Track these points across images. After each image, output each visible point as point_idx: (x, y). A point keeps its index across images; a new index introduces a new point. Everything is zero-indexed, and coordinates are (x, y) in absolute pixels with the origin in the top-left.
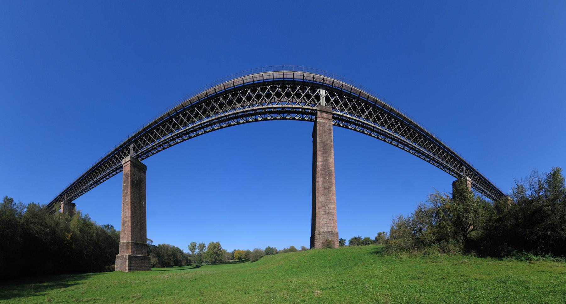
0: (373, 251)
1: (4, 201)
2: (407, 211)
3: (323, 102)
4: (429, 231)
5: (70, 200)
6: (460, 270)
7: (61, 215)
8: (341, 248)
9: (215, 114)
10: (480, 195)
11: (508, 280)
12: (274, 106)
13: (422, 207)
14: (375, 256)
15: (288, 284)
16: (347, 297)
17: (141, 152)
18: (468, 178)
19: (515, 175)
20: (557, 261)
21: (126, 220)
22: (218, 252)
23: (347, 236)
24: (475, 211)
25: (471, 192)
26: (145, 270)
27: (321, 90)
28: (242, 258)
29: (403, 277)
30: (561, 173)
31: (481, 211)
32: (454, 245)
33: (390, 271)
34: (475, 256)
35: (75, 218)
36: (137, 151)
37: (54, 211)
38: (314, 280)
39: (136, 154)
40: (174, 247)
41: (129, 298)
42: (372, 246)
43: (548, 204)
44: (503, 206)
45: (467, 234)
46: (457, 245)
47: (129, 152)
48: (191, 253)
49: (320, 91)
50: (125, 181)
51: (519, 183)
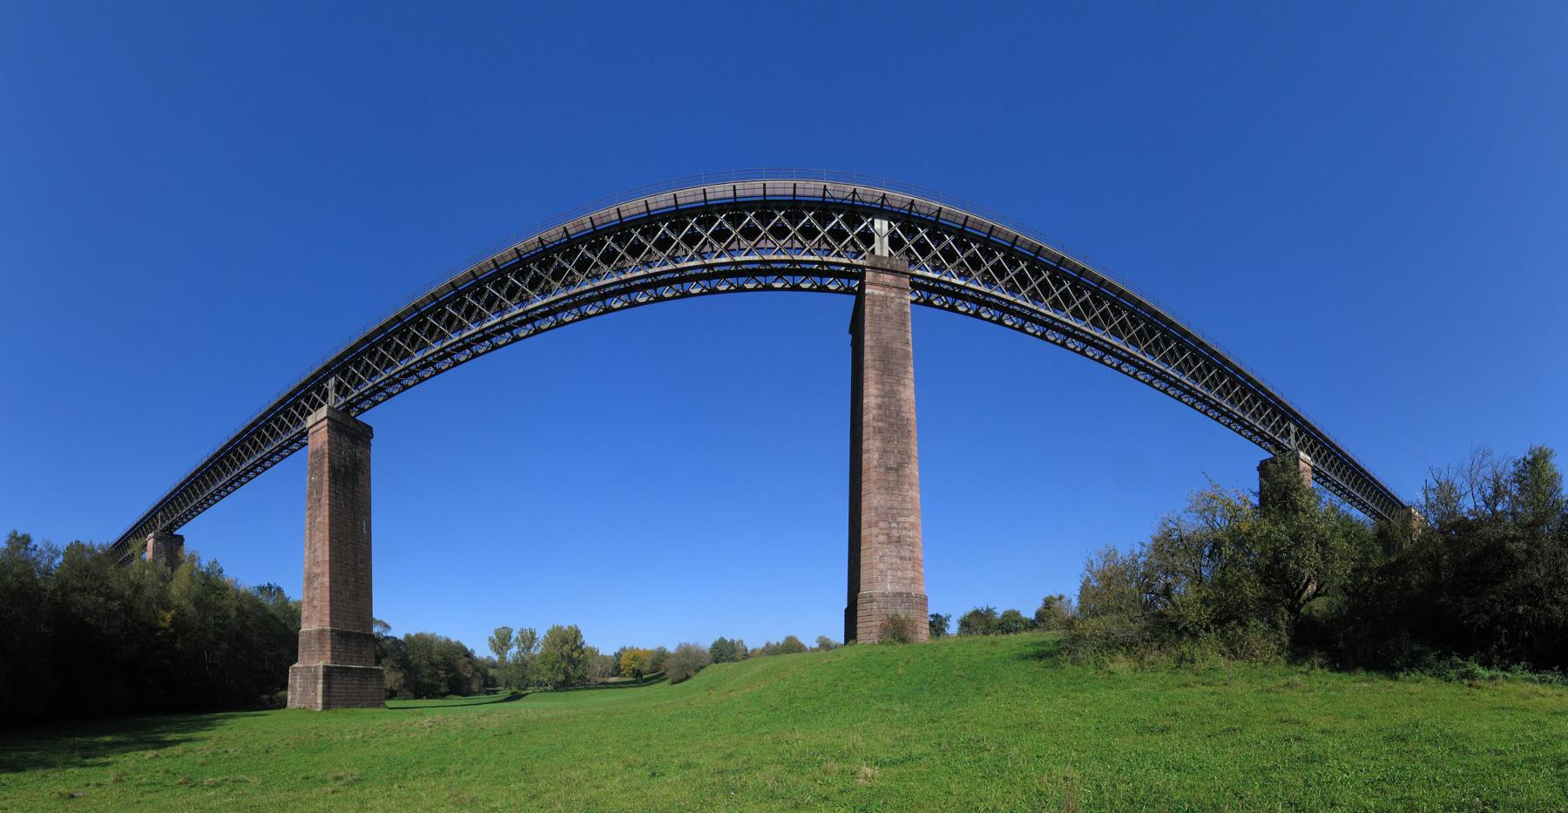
0: (1030, 650)
1: (9, 543)
2: (1130, 536)
3: (882, 247)
4: (1192, 596)
5: (171, 528)
6: (1279, 706)
7: (147, 567)
8: (934, 642)
9: (564, 285)
10: (1336, 500)
11: (1413, 733)
12: (737, 259)
13: (1171, 526)
14: (1035, 665)
15: (780, 748)
16: (953, 786)
17: (356, 393)
18: (1302, 454)
19: (1434, 454)
20: (1541, 681)
21: (317, 570)
22: (575, 654)
23: (955, 610)
24: (1323, 544)
25: (1311, 493)
26: (369, 705)
27: (877, 222)
28: (645, 671)
29: (1117, 727)
30: (1552, 461)
31: (1339, 543)
32: (1264, 637)
33: (1079, 709)
34: (1322, 667)
35: (183, 571)
36: (346, 392)
37: (130, 558)
38: (855, 738)
39: (342, 401)
40: (448, 640)
41: (324, 782)
42: (1025, 636)
43: (1519, 534)
44: (1398, 534)
45: (1301, 606)
46: (1272, 636)
47: (325, 398)
48: (496, 658)
49: (872, 223)
50: (312, 470)
51: (1443, 476)
